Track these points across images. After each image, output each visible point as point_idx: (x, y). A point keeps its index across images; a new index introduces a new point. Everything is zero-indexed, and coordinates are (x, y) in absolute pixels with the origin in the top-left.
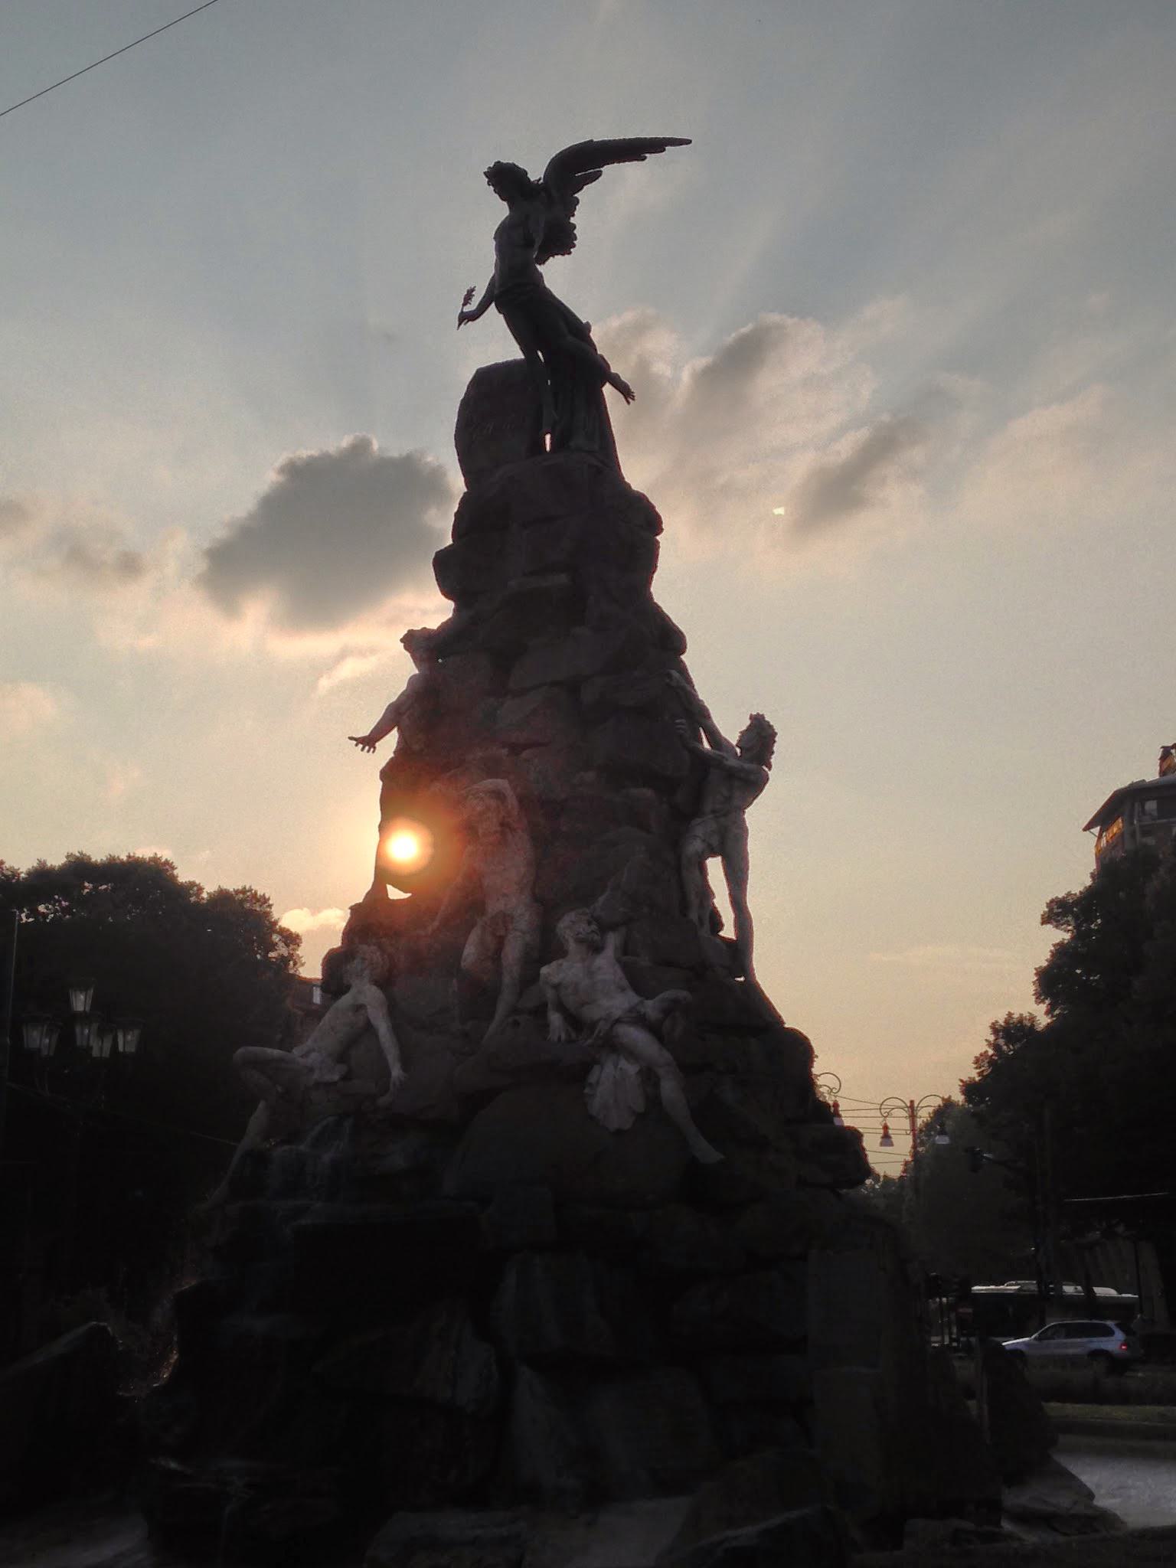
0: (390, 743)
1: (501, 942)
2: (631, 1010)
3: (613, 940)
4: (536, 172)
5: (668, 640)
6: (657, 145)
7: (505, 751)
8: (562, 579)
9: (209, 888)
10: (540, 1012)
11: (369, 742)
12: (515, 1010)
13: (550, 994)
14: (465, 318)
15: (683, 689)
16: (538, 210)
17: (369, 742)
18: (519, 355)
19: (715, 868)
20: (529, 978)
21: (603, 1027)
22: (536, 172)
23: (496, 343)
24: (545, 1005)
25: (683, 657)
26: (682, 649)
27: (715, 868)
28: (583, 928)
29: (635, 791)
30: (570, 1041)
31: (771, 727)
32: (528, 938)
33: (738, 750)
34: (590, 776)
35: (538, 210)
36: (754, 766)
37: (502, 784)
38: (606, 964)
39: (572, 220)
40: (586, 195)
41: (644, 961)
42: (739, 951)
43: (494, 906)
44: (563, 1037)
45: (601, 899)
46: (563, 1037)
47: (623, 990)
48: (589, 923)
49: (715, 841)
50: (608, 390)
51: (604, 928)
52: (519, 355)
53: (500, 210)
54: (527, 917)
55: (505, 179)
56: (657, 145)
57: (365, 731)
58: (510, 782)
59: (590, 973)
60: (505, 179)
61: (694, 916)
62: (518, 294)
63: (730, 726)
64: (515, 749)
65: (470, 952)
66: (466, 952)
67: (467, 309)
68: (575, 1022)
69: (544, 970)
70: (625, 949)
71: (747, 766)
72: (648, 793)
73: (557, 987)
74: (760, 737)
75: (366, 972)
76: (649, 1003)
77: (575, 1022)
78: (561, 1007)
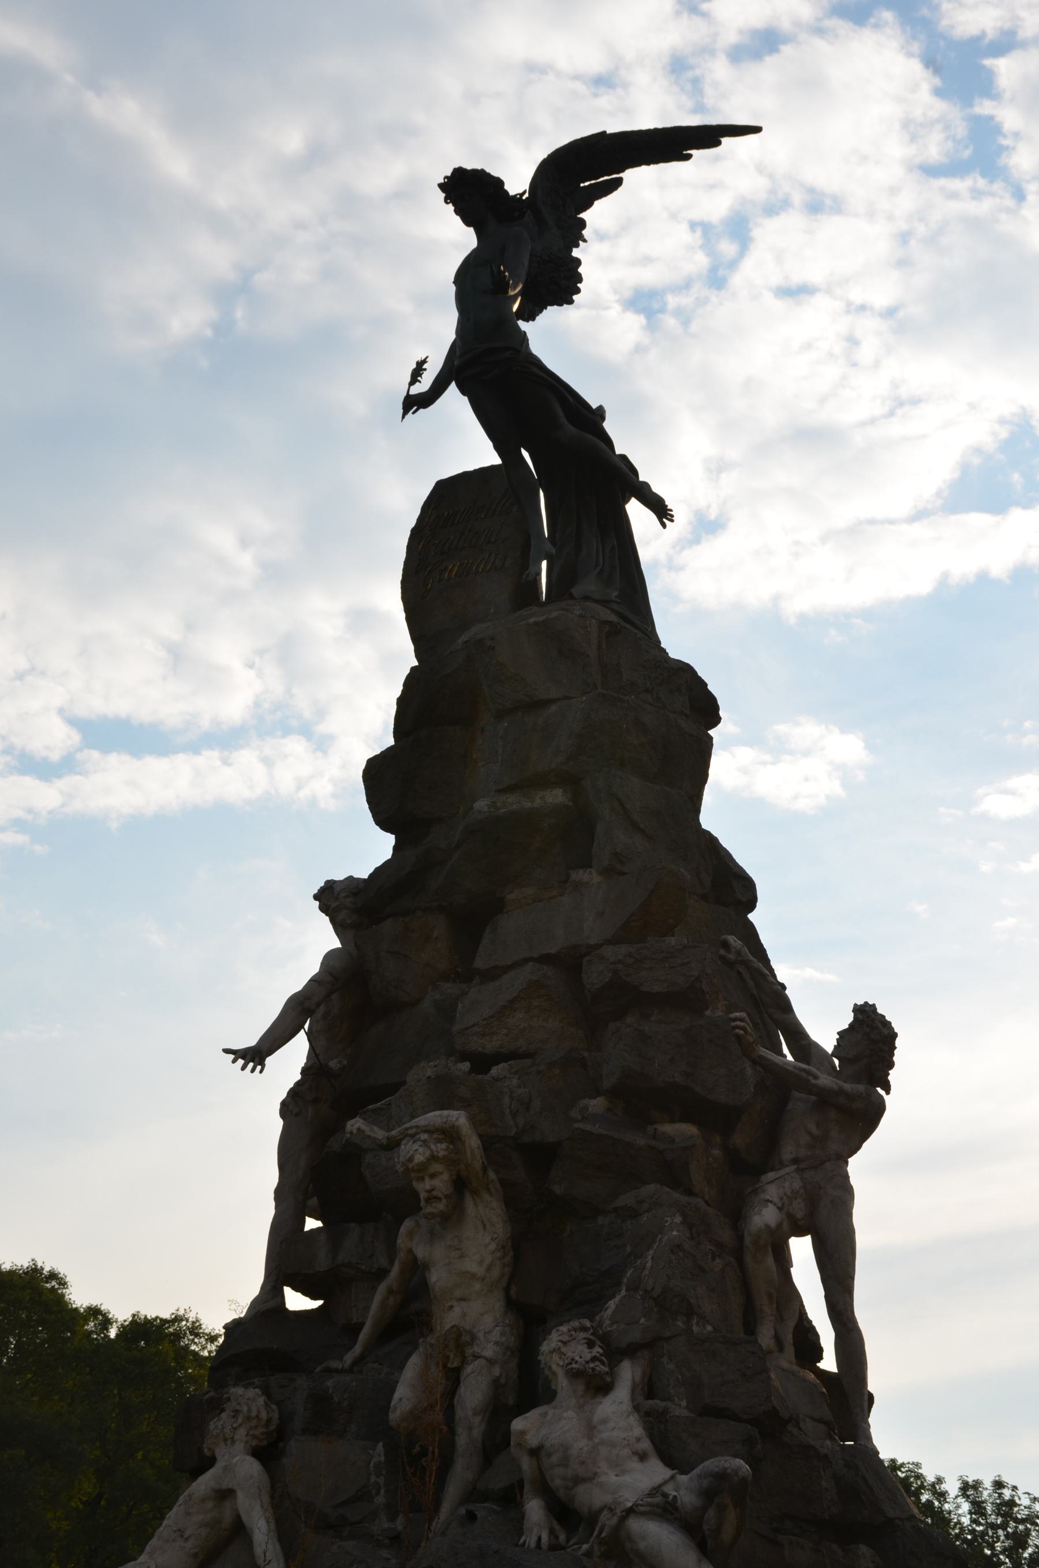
0: (293, 1058)
1: (454, 1377)
2: (655, 1491)
3: (628, 1373)
4: (518, 181)
5: (731, 889)
6: (709, 136)
7: (466, 1066)
8: (556, 797)
9: (121, 1313)
10: (510, 1499)
11: (255, 1056)
12: (474, 1494)
13: (526, 1464)
14: (413, 403)
15: (764, 976)
16: (523, 238)
17: (255, 1056)
18: (494, 459)
19: (801, 1250)
20: (496, 1442)
21: (607, 1521)
22: (518, 181)
23: (462, 442)
24: (521, 1483)
25: (751, 916)
26: (751, 903)
27: (801, 1250)
28: (580, 1353)
29: (668, 1128)
30: (554, 1547)
31: (887, 1025)
32: (497, 1371)
33: (836, 1062)
34: (597, 1104)
35: (523, 238)
36: (861, 1088)
37: (459, 1118)
38: (617, 1409)
39: (576, 253)
40: (597, 216)
41: (680, 1409)
42: (848, 1396)
43: (450, 1318)
44: (545, 1538)
45: (612, 1304)
46: (545, 1538)
47: (642, 1457)
48: (590, 1345)
49: (799, 1209)
50: (635, 510)
51: (615, 1353)
52: (494, 459)
53: (460, 239)
54: (495, 1336)
55: (470, 192)
56: (709, 136)
57: (250, 1039)
58: (471, 1118)
59: (590, 1429)
60: (470, 192)
61: (765, 1337)
62: (492, 367)
63: (824, 1026)
64: (482, 1063)
65: (404, 1394)
66: (397, 1396)
67: (416, 390)
68: (564, 1513)
69: (518, 1424)
70: (649, 1388)
71: (848, 1087)
72: (689, 1129)
73: (535, 1452)
74: (871, 1039)
75: (241, 1433)
76: (683, 1479)
77: (564, 1513)
78: (545, 1490)
